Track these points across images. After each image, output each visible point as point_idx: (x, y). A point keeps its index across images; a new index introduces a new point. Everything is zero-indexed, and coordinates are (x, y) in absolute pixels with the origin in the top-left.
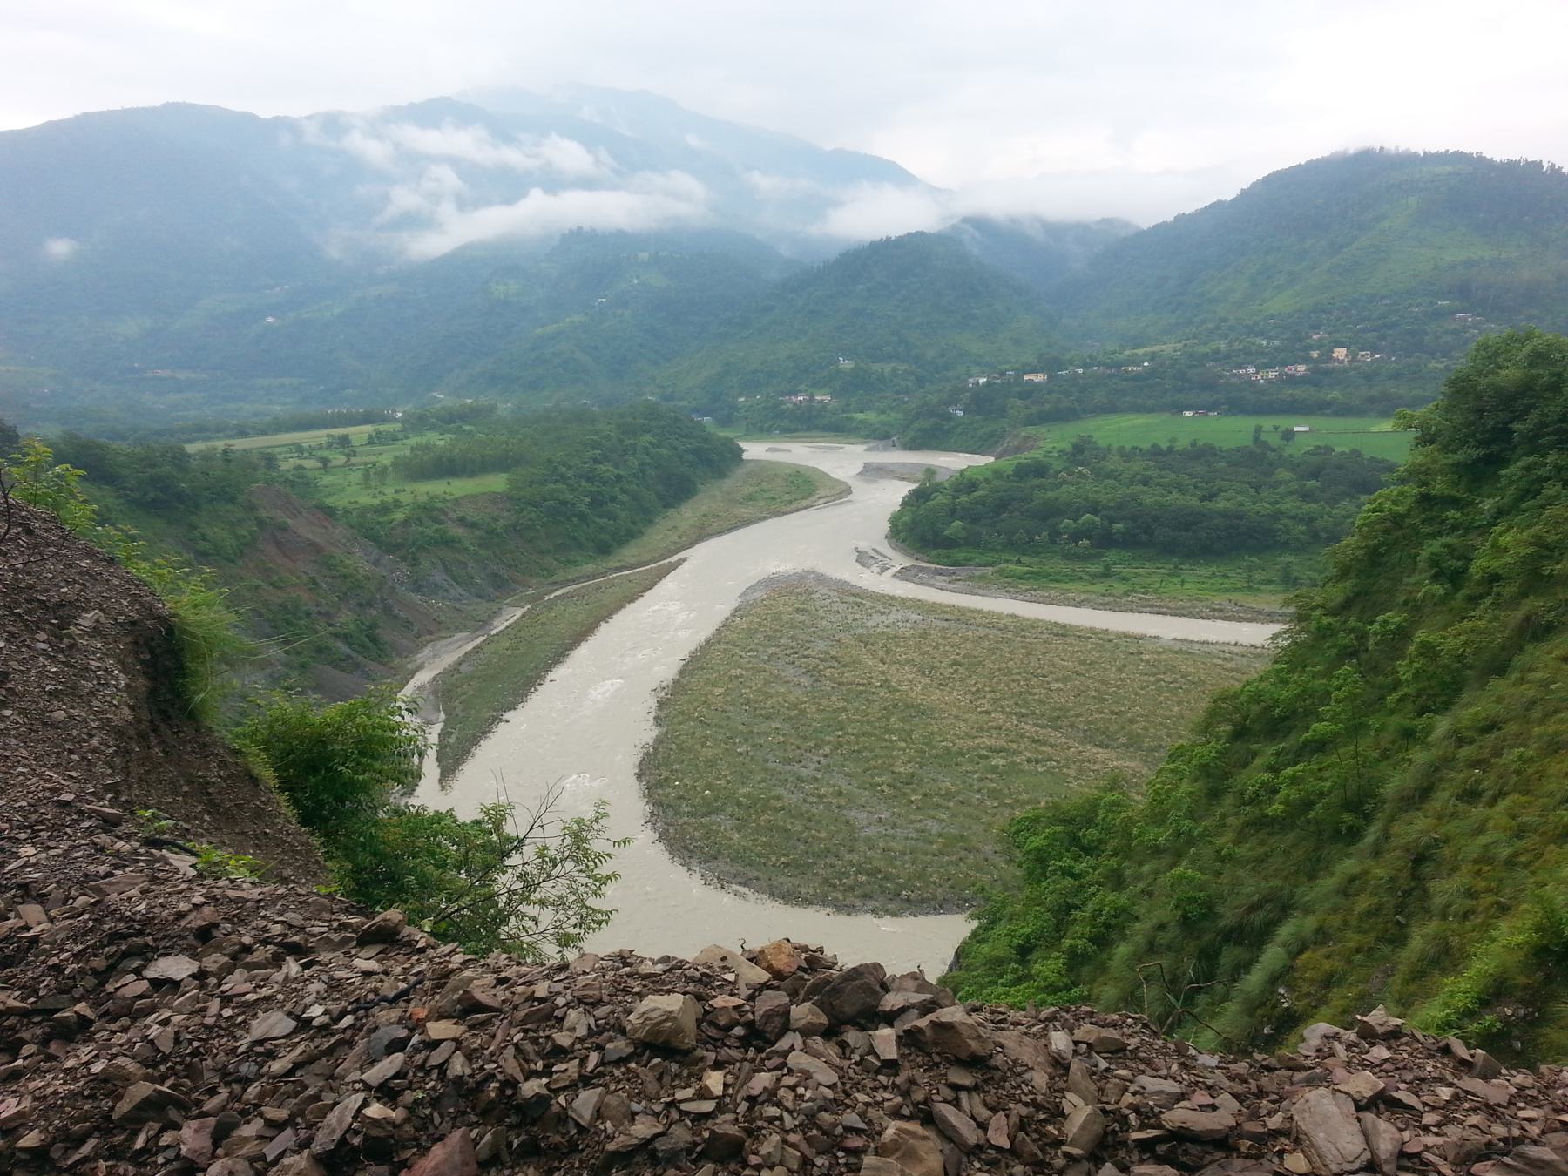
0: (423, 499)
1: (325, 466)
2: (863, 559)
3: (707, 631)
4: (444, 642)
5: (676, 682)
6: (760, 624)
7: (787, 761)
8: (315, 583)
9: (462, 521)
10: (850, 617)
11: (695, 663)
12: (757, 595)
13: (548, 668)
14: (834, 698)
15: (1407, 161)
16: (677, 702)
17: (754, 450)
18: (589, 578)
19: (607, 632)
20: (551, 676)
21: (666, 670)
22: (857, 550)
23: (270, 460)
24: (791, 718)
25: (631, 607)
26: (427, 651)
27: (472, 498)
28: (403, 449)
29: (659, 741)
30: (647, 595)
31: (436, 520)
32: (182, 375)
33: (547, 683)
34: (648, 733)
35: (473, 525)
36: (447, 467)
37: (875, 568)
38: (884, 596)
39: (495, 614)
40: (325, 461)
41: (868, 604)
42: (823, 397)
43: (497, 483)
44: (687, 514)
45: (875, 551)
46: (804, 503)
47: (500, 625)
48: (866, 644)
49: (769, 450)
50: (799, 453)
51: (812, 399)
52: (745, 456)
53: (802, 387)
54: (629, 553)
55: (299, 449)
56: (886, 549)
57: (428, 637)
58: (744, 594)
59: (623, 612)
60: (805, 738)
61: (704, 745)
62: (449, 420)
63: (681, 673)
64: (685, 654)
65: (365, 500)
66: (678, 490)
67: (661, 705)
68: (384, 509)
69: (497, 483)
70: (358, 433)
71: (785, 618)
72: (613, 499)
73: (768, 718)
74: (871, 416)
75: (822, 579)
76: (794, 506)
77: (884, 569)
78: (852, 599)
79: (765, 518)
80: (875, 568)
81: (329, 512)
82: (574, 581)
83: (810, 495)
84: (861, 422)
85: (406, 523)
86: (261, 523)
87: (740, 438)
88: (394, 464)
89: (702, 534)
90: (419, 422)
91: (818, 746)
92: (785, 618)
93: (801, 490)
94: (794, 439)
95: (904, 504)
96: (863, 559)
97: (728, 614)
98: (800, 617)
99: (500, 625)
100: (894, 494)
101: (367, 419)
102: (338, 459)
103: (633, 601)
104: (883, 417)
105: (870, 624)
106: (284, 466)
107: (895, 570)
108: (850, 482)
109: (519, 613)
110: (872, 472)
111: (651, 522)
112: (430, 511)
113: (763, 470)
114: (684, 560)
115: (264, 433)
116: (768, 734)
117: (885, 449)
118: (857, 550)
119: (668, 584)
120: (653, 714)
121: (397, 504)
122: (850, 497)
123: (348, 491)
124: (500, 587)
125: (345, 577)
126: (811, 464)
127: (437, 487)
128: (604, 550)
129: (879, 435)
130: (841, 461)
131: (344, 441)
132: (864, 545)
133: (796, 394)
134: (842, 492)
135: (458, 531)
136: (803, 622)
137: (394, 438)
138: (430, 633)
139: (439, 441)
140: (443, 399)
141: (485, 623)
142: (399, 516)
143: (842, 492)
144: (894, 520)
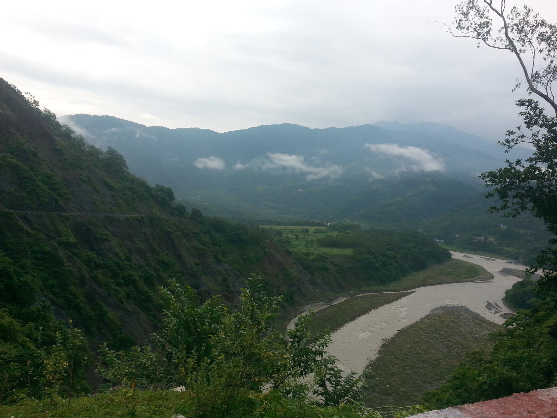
0: (322, 253)
1: (297, 238)
2: (489, 306)
3: (412, 321)
4: (315, 304)
5: (392, 338)
6: (434, 324)
7: (425, 382)
8: (277, 275)
9: (332, 263)
10: (474, 329)
11: (403, 333)
12: (438, 312)
13: (347, 322)
14: (455, 361)
15: (89, 116)
16: (389, 348)
17: (457, 255)
18: (374, 292)
19: (373, 313)
20: (347, 325)
21: (391, 333)
22: (487, 302)
23: (280, 233)
24: (434, 365)
25: (386, 306)
26: (308, 306)
27: (338, 256)
28: (322, 236)
29: (377, 360)
30: (394, 302)
31: (323, 261)
32: (271, 204)
33: (344, 327)
34: (374, 356)
35: (337, 265)
36: (334, 244)
37: (493, 311)
38: (493, 323)
39: (336, 298)
40: (297, 236)
41: (484, 325)
42: (491, 239)
43: (348, 252)
44: (421, 275)
45: (496, 304)
46: (471, 279)
47: (336, 302)
48: (478, 341)
49: (464, 256)
50: (476, 260)
51: (486, 239)
52: (452, 257)
53: (483, 234)
54: (393, 285)
55: (292, 231)
56: (501, 304)
57: (311, 301)
58: (432, 310)
59: (382, 307)
60: (436, 374)
61: (393, 366)
62: (344, 228)
63: (396, 335)
64: (400, 328)
65: (304, 251)
66: (418, 265)
67: (383, 346)
68: (308, 255)
69: (348, 252)
70: (312, 229)
71: (446, 323)
72: (391, 264)
73: (424, 362)
74: (511, 249)
75: (467, 311)
76: (466, 280)
77: (497, 312)
78: (478, 322)
79: (452, 282)
80: (493, 311)
81: (289, 253)
82: (368, 292)
83: (475, 276)
84: (506, 251)
85: (313, 260)
86: (265, 253)
87: (452, 250)
88: (317, 241)
89: (424, 284)
90: (333, 228)
91: (440, 379)
92: (446, 323)
93: (473, 274)
94: (475, 254)
95: (514, 286)
96: (489, 306)
97: (423, 317)
98: (452, 324)
99: (336, 302)
100: (510, 282)
101: (318, 224)
102: (301, 236)
103: (387, 303)
104: (517, 250)
105: (482, 333)
106: (284, 236)
107: (502, 313)
108: (494, 274)
109: (345, 299)
110: (506, 272)
111: (405, 276)
112: (322, 258)
113: (458, 263)
114: (414, 292)
115: (286, 225)
116: (421, 369)
117: (515, 263)
118: (487, 302)
119: (404, 300)
120: (379, 349)
121: (313, 254)
122: (492, 280)
123: (300, 248)
124: (340, 289)
125: (288, 275)
126: (480, 264)
127: (328, 250)
128: (383, 282)
129: (514, 258)
130: (493, 265)
131: (307, 231)
132: (491, 301)
133: (480, 236)
134: (489, 277)
135: (330, 266)
136: (453, 327)
137: (323, 232)
138: (312, 300)
139: (335, 234)
140: (347, 221)
141: (332, 300)
142: (312, 258)
143: (489, 277)
144: (507, 292)
